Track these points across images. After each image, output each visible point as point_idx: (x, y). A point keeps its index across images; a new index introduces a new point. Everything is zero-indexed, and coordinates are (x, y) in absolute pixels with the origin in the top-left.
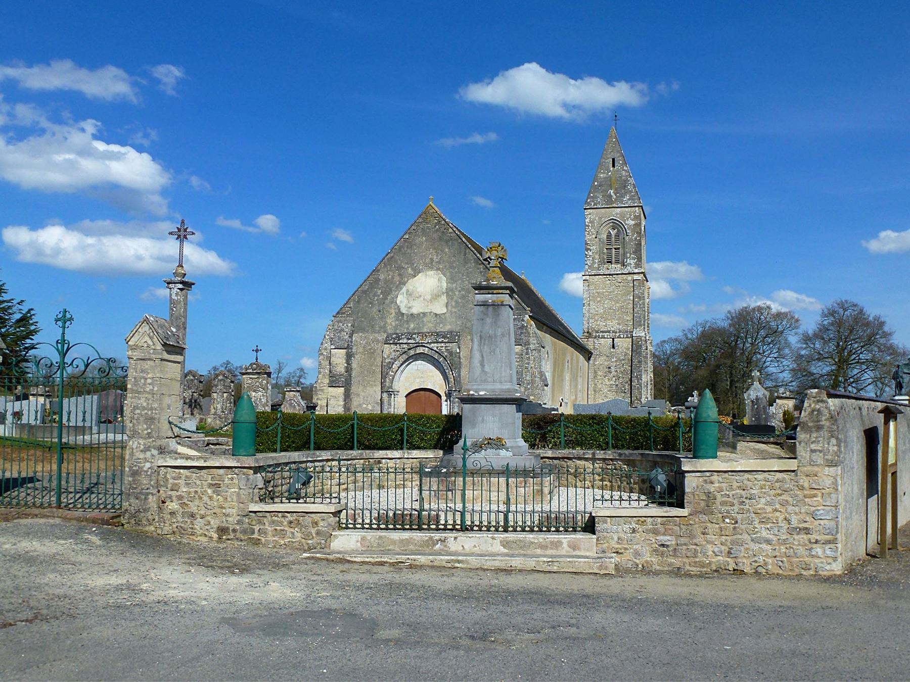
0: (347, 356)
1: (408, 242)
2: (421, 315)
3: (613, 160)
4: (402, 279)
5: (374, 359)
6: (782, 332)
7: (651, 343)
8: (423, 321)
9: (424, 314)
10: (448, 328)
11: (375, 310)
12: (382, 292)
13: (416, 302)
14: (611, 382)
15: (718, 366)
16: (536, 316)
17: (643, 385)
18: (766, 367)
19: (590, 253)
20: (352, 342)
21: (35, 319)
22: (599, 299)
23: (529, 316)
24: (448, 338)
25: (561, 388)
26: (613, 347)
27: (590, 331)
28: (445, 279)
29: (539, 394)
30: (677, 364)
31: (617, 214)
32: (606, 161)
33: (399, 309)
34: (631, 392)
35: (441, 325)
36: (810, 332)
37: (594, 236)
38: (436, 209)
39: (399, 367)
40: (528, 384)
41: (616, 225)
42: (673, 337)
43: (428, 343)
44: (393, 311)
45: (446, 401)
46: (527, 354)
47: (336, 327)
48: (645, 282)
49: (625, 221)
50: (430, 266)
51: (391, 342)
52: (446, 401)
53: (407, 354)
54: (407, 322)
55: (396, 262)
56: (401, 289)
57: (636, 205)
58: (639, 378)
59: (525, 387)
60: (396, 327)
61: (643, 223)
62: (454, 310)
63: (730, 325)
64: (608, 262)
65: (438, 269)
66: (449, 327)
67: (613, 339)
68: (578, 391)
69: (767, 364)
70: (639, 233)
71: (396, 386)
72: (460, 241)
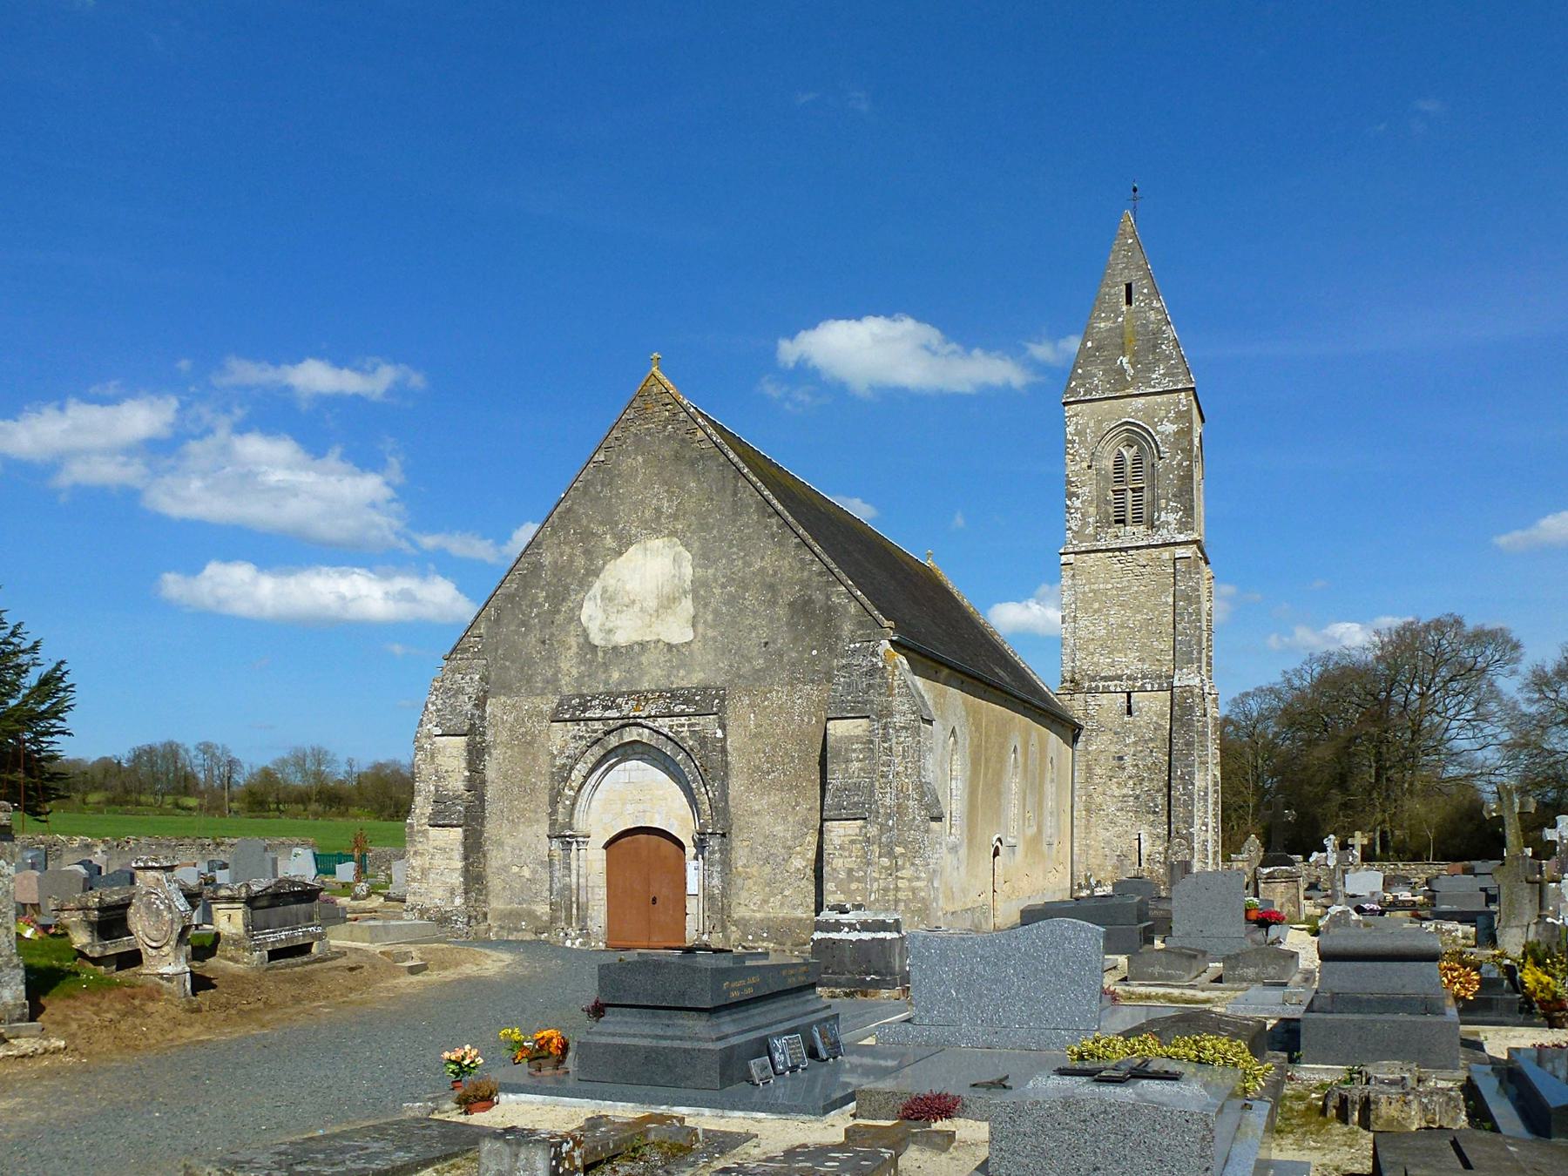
0: (470, 752)
1: (604, 471)
2: (636, 648)
3: (1129, 287)
4: (591, 560)
5: (533, 759)
6: (1484, 671)
7: (1215, 700)
8: (640, 664)
9: (643, 645)
10: (696, 678)
11: (532, 639)
12: (547, 597)
13: (623, 616)
14: (1125, 791)
15: (1352, 740)
16: (910, 642)
17: (1196, 797)
18: (1450, 740)
19: (1078, 503)
20: (483, 718)
21: (68, 680)
22: (1096, 605)
23: (891, 642)
24: (696, 703)
25: (997, 811)
26: (1129, 712)
27: (1077, 677)
28: (690, 557)
29: (915, 840)
30: (1270, 736)
31: (1137, 410)
32: (1113, 291)
33: (586, 637)
34: (1169, 811)
35: (682, 672)
36: (1550, 668)
37: (1085, 465)
38: (668, 383)
39: (586, 778)
40: (889, 816)
41: (1136, 435)
42: (1264, 684)
43: (649, 717)
44: (573, 641)
45: (696, 858)
46: (885, 739)
47: (448, 684)
48: (1202, 563)
49: (1154, 425)
50: (654, 526)
51: (567, 716)
52: (696, 858)
53: (602, 746)
54: (605, 666)
55: (578, 521)
56: (590, 586)
57: (1180, 386)
58: (1188, 781)
59: (882, 825)
60: (579, 680)
61: (1198, 428)
62: (710, 633)
63: (1378, 658)
64: (1117, 522)
65: (673, 533)
66: (701, 675)
67: (1129, 694)
68: (1046, 813)
69: (1453, 732)
70: (1188, 452)
71: (581, 823)
72: (722, 459)
